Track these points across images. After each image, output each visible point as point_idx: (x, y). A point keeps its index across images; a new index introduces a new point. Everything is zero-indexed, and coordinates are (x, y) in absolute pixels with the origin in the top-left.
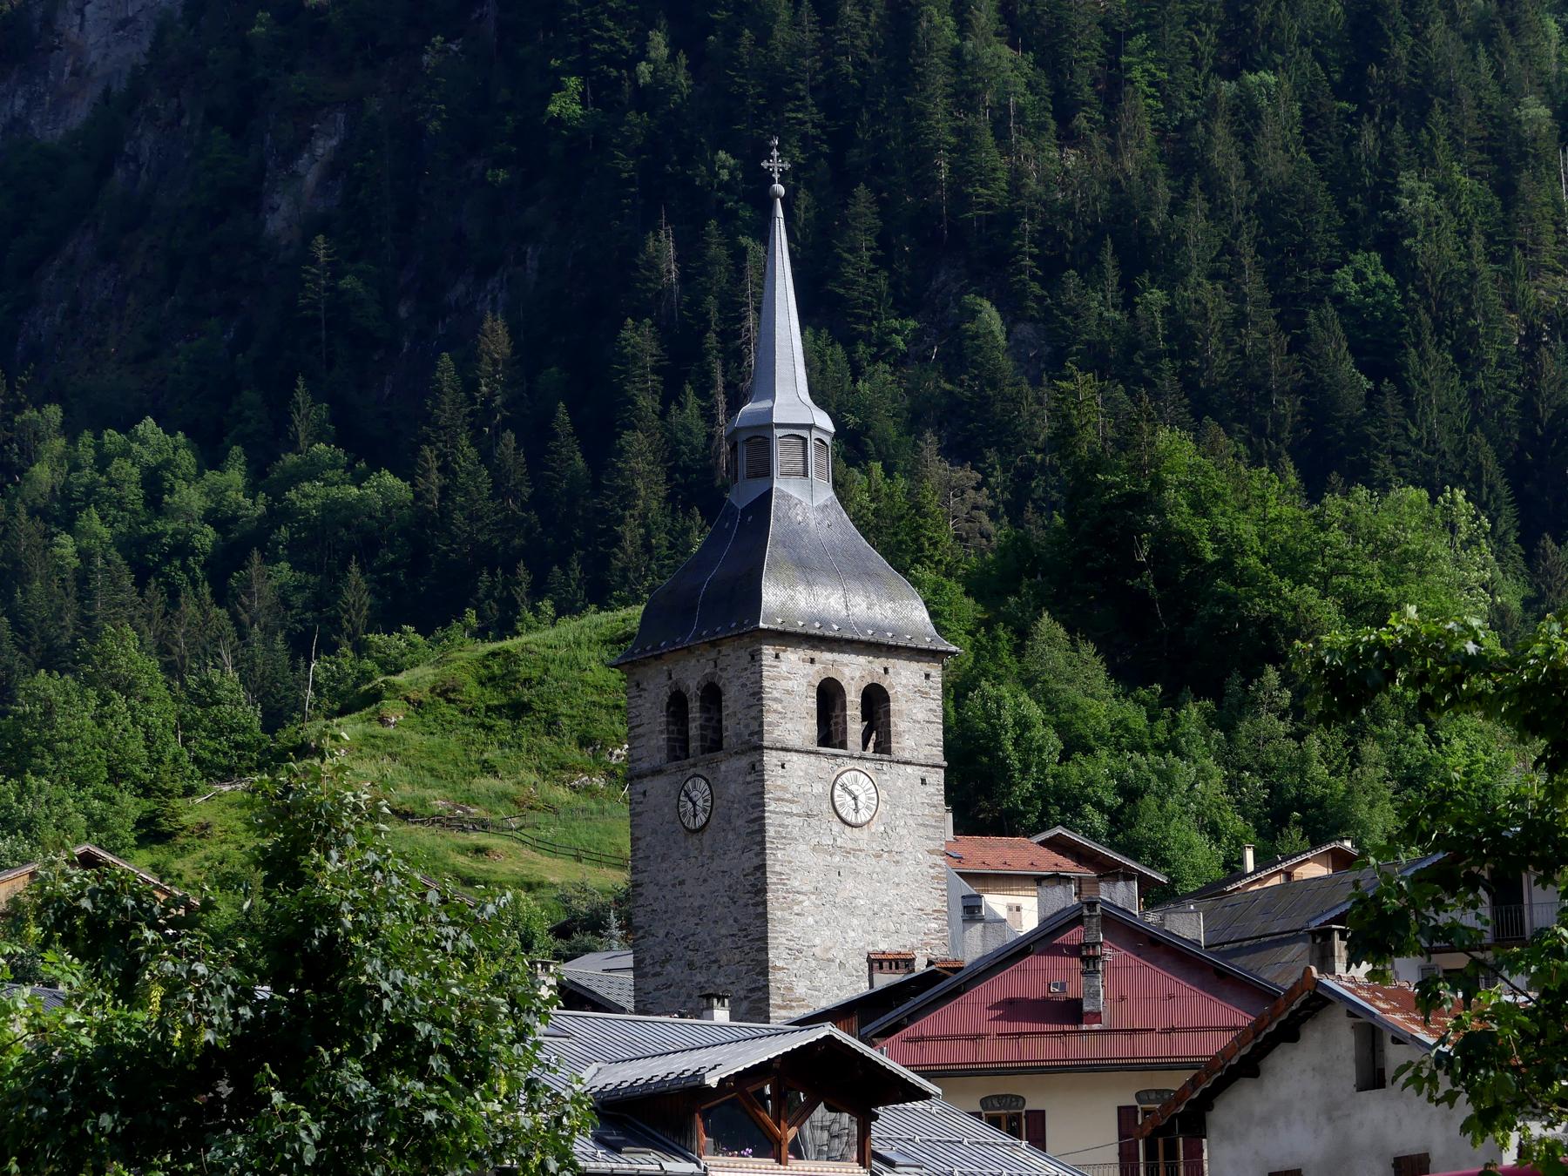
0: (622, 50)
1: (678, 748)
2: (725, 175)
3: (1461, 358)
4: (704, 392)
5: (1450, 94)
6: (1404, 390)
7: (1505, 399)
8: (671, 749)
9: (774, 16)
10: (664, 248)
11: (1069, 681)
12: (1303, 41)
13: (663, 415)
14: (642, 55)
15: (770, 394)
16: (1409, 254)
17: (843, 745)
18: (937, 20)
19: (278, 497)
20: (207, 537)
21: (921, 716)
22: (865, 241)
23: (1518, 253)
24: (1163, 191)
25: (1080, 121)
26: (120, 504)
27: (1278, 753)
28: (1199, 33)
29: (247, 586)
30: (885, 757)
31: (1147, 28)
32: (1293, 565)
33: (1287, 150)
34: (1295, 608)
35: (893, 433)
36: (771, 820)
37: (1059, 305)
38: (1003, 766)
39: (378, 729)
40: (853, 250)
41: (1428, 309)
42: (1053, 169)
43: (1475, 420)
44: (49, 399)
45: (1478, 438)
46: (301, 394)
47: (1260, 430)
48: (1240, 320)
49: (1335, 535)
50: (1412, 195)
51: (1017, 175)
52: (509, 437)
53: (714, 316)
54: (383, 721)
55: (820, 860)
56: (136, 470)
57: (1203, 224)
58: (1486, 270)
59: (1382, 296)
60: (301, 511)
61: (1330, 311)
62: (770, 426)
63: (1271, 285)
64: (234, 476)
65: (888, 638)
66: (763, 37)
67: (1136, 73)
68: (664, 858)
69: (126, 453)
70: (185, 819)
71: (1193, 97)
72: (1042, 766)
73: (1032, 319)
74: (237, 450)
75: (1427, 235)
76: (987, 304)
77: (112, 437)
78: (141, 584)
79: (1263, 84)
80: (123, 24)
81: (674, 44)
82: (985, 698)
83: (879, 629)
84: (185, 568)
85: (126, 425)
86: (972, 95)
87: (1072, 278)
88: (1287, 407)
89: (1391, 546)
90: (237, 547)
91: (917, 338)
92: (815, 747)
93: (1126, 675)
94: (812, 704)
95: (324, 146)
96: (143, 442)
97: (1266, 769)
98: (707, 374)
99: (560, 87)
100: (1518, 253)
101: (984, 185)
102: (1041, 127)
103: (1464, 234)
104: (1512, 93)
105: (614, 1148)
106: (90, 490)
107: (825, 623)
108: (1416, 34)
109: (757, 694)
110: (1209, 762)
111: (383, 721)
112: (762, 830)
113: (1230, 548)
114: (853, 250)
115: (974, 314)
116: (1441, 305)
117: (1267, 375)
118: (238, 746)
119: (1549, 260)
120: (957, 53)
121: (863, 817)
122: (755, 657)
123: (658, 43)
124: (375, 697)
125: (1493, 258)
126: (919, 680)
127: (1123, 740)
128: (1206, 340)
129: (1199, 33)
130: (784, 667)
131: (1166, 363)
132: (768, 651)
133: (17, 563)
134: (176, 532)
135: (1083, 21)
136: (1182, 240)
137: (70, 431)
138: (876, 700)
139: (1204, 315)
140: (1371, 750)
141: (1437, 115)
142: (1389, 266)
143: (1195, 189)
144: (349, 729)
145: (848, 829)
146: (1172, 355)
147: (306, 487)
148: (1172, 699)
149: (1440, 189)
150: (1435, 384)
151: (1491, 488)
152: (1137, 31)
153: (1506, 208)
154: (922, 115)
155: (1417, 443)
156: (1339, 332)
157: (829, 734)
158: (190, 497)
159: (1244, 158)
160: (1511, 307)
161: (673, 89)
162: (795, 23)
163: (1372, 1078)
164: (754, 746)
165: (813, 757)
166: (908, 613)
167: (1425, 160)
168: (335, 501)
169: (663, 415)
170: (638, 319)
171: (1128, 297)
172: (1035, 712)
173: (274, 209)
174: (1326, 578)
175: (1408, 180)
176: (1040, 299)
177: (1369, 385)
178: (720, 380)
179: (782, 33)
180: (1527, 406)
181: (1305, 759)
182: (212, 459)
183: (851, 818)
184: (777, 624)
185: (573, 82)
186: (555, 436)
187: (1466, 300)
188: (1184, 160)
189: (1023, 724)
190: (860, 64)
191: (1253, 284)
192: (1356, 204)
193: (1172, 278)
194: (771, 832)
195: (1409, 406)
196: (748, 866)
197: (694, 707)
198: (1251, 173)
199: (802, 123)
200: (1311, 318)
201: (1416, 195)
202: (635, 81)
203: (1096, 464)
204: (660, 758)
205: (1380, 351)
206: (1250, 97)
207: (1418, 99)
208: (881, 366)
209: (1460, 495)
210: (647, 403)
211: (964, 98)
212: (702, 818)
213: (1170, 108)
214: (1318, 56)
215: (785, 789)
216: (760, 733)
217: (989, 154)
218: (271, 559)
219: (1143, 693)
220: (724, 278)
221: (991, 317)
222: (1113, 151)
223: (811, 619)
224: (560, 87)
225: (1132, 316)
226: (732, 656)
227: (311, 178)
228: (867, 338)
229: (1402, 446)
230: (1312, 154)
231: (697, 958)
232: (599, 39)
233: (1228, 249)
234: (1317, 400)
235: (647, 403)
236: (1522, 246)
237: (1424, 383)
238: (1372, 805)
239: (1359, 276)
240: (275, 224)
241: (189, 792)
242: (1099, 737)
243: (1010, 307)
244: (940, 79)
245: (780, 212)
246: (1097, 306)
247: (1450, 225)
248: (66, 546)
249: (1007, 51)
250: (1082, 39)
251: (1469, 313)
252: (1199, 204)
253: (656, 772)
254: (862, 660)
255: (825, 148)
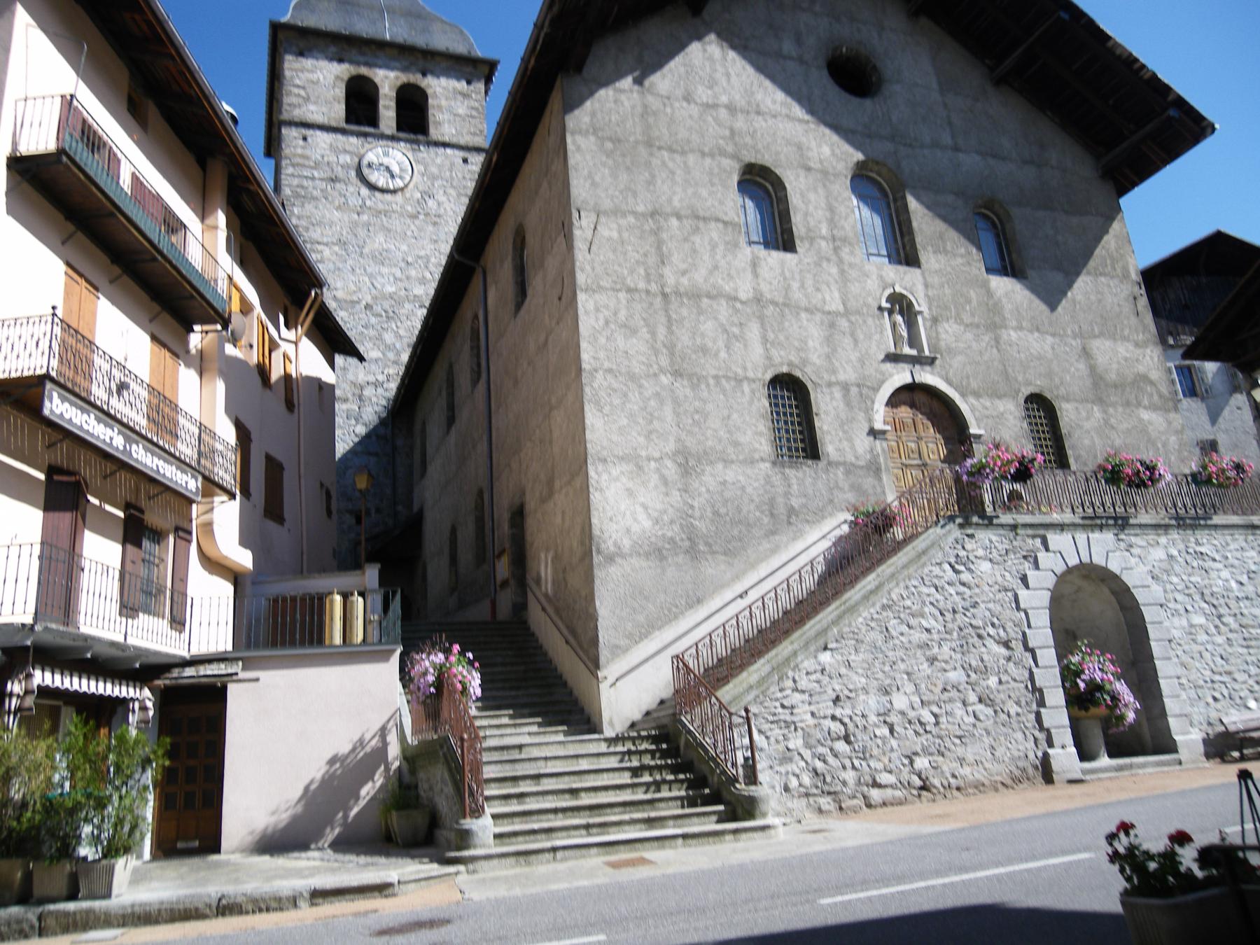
30: (421, 137)
92: (343, 125)
145: (378, 194)
165: (339, 137)
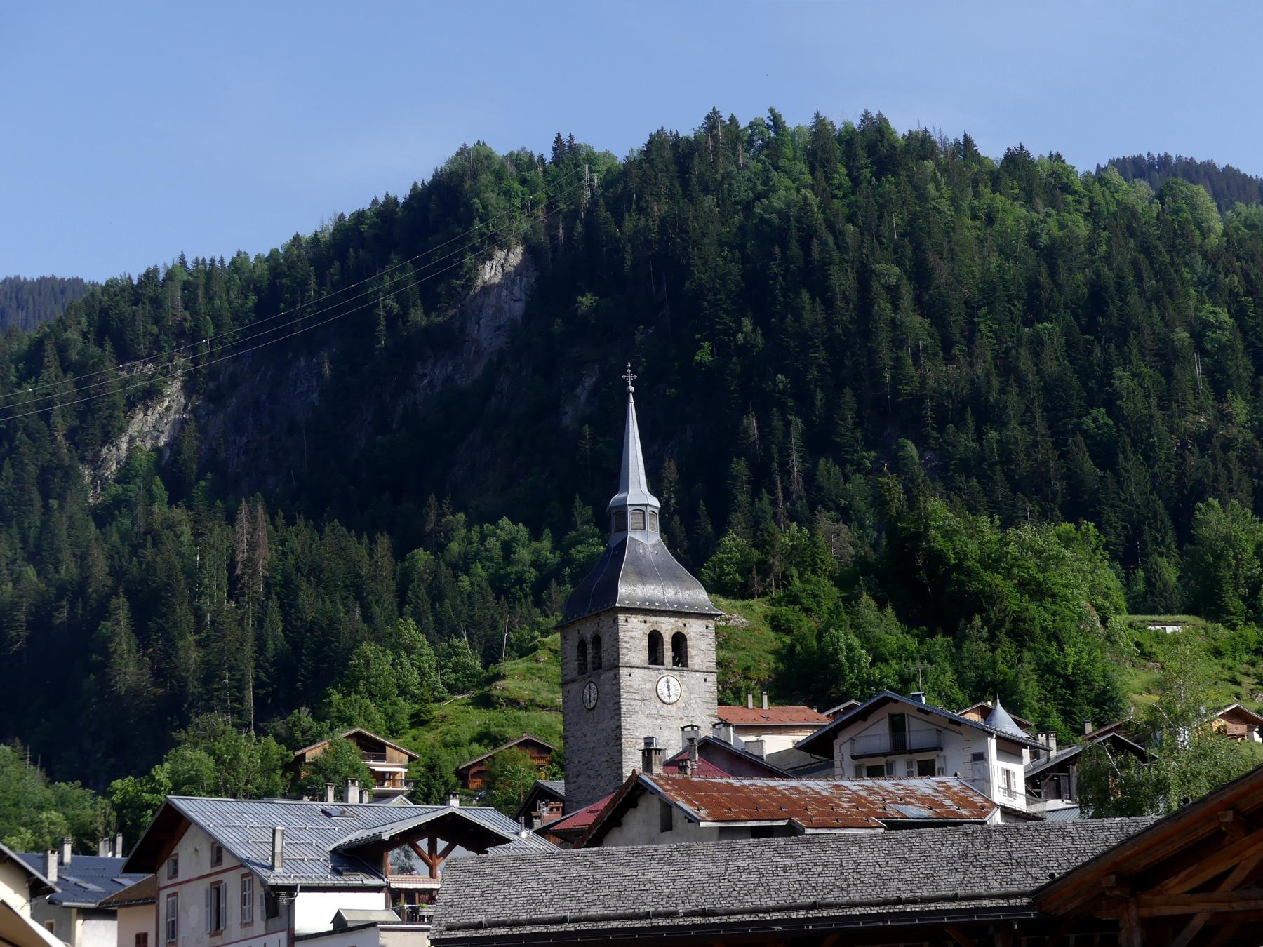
0: (730, 328)
1: (582, 669)
2: (781, 386)
3: (1147, 458)
4: (772, 492)
5: (1138, 328)
6: (1117, 475)
7: (1169, 477)
8: (580, 669)
9: (803, 308)
10: (751, 423)
11: (878, 626)
12: (1066, 307)
13: (752, 504)
14: (740, 330)
15: (628, 491)
16: (1120, 408)
17: (663, 664)
18: (882, 305)
19: (566, 552)
20: (532, 574)
21: (703, 647)
22: (849, 415)
23: (1174, 405)
24: (995, 383)
25: (955, 351)
26: (491, 559)
27: (982, 658)
28: (1014, 305)
29: (550, 596)
31: (987, 304)
32: (991, 563)
33: (1058, 359)
34: (990, 585)
35: (863, 507)
36: (623, 702)
37: (945, 441)
38: (840, 668)
39: (534, 665)
40: (844, 419)
41: (1129, 435)
42: (941, 375)
43: (1154, 488)
44: (459, 510)
45: (1154, 497)
46: (578, 502)
47: (1045, 499)
48: (1035, 444)
49: (1012, 548)
50: (1120, 379)
51: (924, 378)
52: (677, 518)
53: (776, 455)
54: (537, 661)
55: (650, 721)
56: (498, 544)
57: (1016, 398)
58: (1158, 414)
59: (1106, 430)
60: (575, 559)
61: (1079, 438)
62: (626, 506)
63: (1050, 427)
64: (547, 543)
65: (686, 609)
66: (798, 317)
67: (982, 326)
68: (577, 724)
69: (494, 535)
70: (435, 713)
71: (1011, 336)
72: (860, 669)
73: (932, 449)
74: (547, 531)
75: (1128, 398)
76: (909, 443)
77: (488, 527)
78: (497, 598)
79: (1046, 328)
80: (498, 328)
81: (755, 325)
82: (832, 636)
83: (681, 604)
84: (521, 589)
85: (494, 522)
86: (902, 341)
87: (951, 428)
88: (1059, 486)
89: (1041, 552)
90: (546, 576)
91: (875, 461)
93: (908, 620)
94: (645, 643)
95: (589, 382)
96: (502, 529)
97: (977, 668)
98: (774, 483)
99: (701, 347)
100: (1174, 405)
101: (907, 384)
102: (936, 355)
103: (1147, 397)
104: (1169, 326)
105: (340, 873)
106: (477, 554)
107: (652, 603)
108: (1122, 300)
109: (616, 639)
110: (946, 665)
111: (537, 661)
112: (619, 708)
113: (962, 557)
114: (844, 419)
115: (903, 448)
116: (1136, 432)
117: (1049, 471)
118: (468, 676)
119: (1190, 408)
120: (893, 321)
121: (673, 699)
122: (615, 621)
123: (747, 324)
124: (535, 648)
125: (1161, 408)
126: (703, 629)
127: (903, 654)
128: (1018, 454)
129: (1014, 305)
130: (630, 625)
131: (998, 468)
132: (621, 617)
133: (440, 591)
134: (517, 572)
135: (955, 302)
136: (1006, 407)
137: (469, 526)
138: (679, 641)
139: (1016, 443)
140: (1027, 655)
141: (1132, 339)
142: (1110, 415)
143: (1012, 381)
144: (522, 664)
146: (1002, 463)
147: (579, 547)
148: (932, 634)
149: (1134, 375)
150: (1133, 472)
151: (1162, 522)
152: (983, 306)
153: (1169, 383)
154: (876, 352)
155: (1124, 501)
156: (1085, 448)
157: (655, 656)
158: (524, 555)
159: (1036, 365)
160: (1172, 432)
161: (754, 346)
162: (814, 311)
163: (667, 826)
164: (615, 666)
166: (699, 596)
167: (1127, 361)
168: (593, 553)
169: (752, 504)
170: (739, 458)
171: (980, 436)
172: (857, 642)
173: (566, 413)
174: (1009, 570)
175: (1118, 372)
176: (936, 439)
177: (1101, 474)
178: (779, 486)
179: (807, 315)
180: (1180, 480)
181: (994, 662)
182: (536, 535)
183: (667, 700)
184: (626, 604)
185: (707, 344)
186: (699, 517)
187: (1148, 429)
188: (1006, 368)
189: (850, 648)
190: (845, 328)
191: (1041, 426)
192: (1092, 384)
193: (1001, 425)
194: (624, 709)
195: (1120, 483)
196: (614, 726)
197: (589, 646)
198: (1039, 372)
199: (817, 358)
200: (1070, 441)
201: (1122, 379)
202: (736, 343)
203: (899, 517)
204: (574, 674)
205: (1105, 455)
206: (1039, 335)
207: (1123, 332)
208: (858, 475)
209: (1091, 525)
210: (743, 499)
211: (898, 343)
212: (593, 703)
213: (1000, 342)
214: (1073, 313)
215: (631, 687)
216: (618, 659)
217: (910, 370)
218: (561, 583)
219: (915, 631)
220: (781, 436)
221: (911, 449)
222: (971, 365)
223: (644, 601)
224: (701, 347)
225: (981, 445)
226: (606, 620)
227: (583, 398)
228: (851, 462)
229: (1117, 503)
230: (1071, 362)
231: (591, 773)
232: (720, 324)
233: (1028, 409)
234: (1074, 480)
235: (743, 499)
236: (1177, 401)
237: (1127, 471)
238: (1027, 683)
239: (1095, 420)
240: (567, 421)
241: (441, 700)
242: (891, 654)
243: (922, 443)
244: (884, 334)
245: (632, 400)
246: (965, 441)
247: (1139, 394)
248: (465, 581)
249: (918, 319)
250: (955, 311)
251: (1151, 436)
252: (1014, 389)
253: (573, 681)
254: (672, 620)
255: (829, 370)
